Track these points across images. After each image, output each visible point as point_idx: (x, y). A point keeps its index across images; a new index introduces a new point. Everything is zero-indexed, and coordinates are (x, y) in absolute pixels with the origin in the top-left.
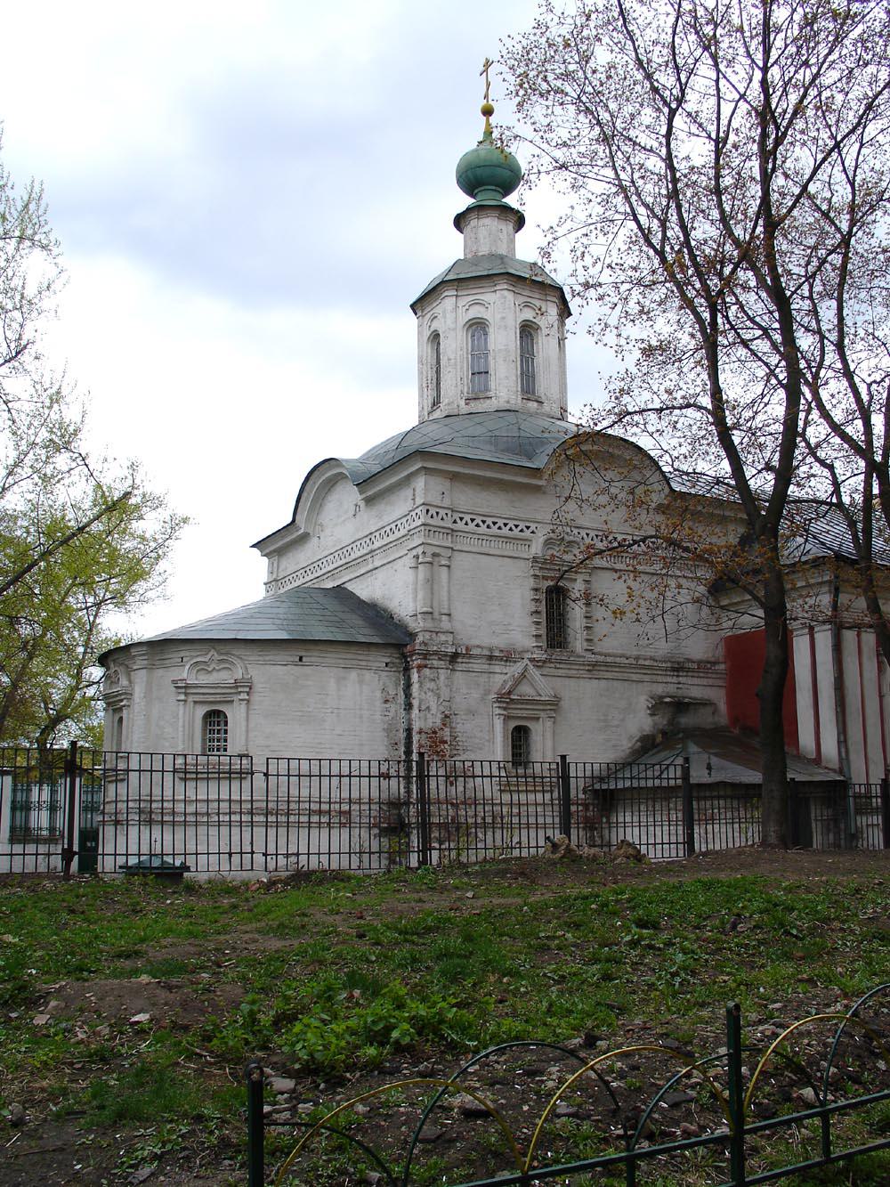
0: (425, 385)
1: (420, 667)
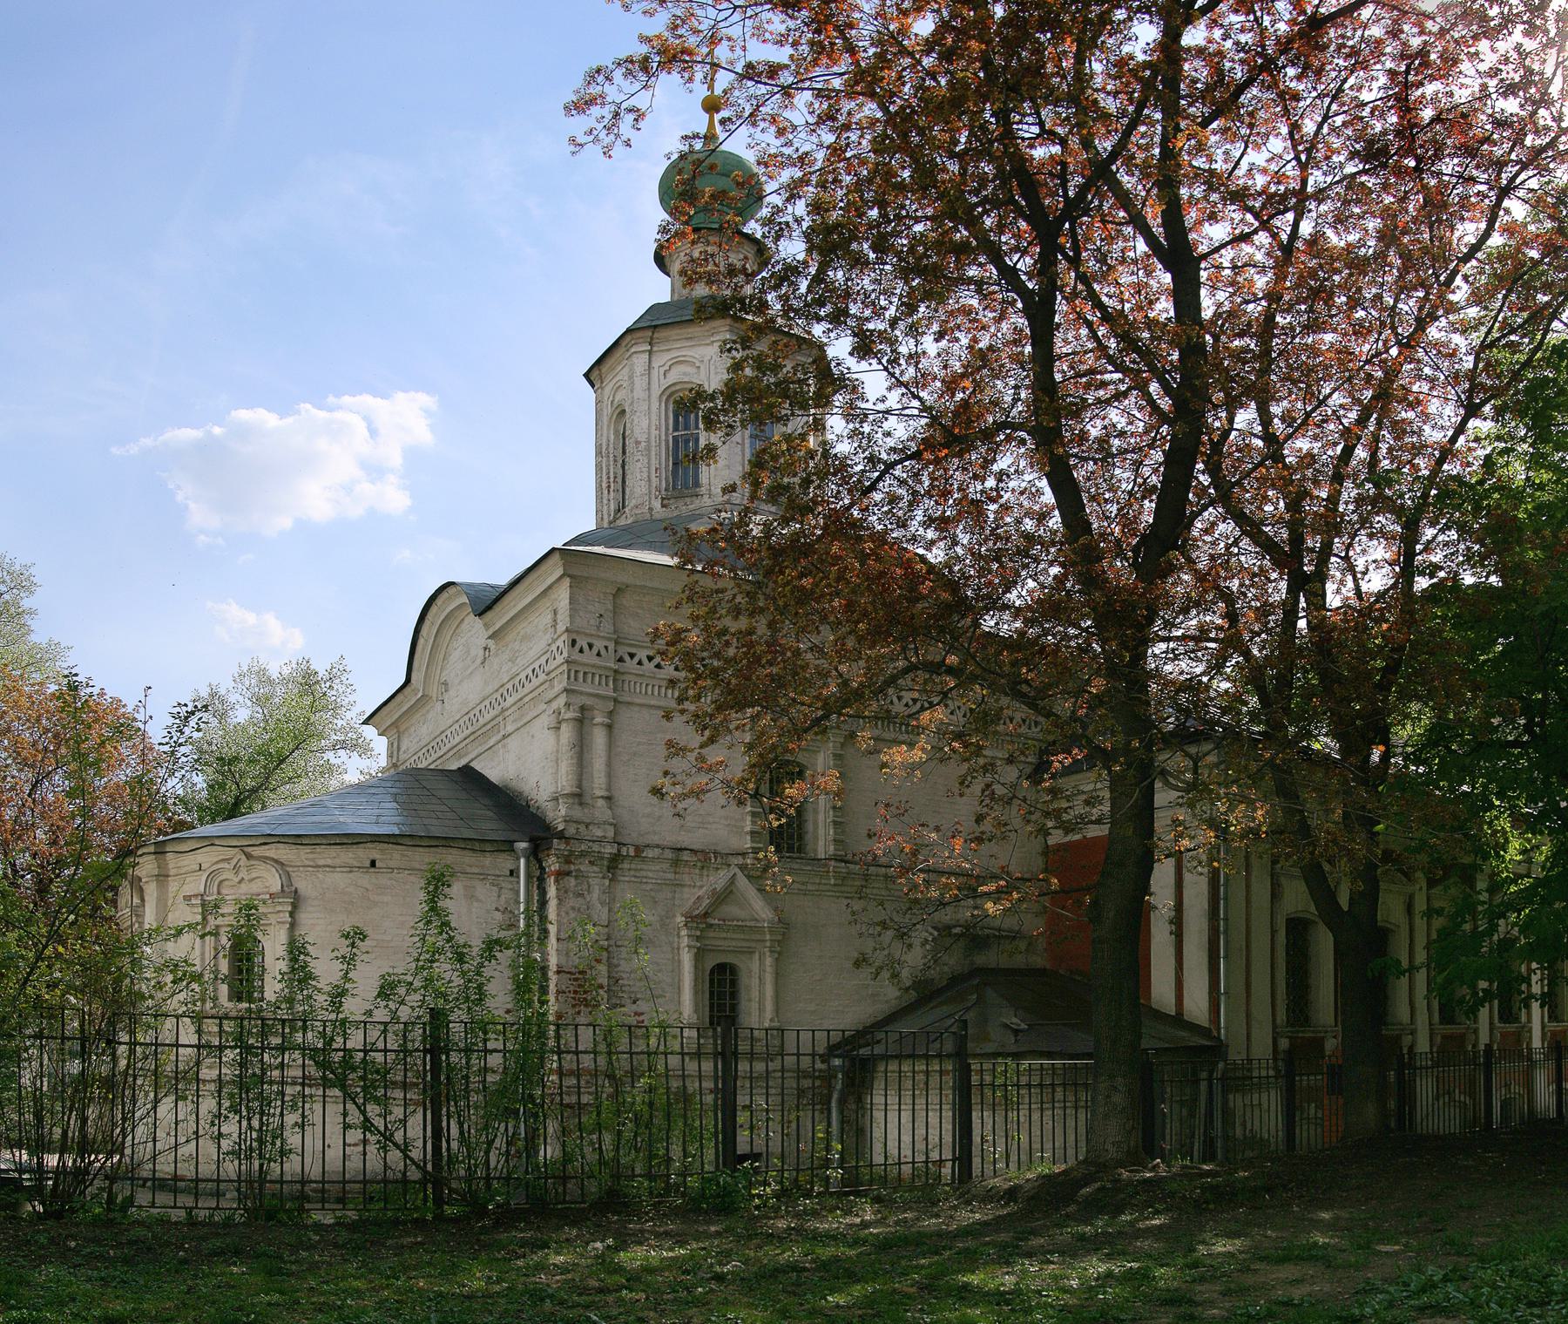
0: (604, 485)
1: (560, 875)
